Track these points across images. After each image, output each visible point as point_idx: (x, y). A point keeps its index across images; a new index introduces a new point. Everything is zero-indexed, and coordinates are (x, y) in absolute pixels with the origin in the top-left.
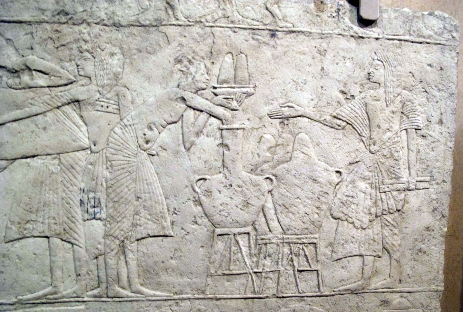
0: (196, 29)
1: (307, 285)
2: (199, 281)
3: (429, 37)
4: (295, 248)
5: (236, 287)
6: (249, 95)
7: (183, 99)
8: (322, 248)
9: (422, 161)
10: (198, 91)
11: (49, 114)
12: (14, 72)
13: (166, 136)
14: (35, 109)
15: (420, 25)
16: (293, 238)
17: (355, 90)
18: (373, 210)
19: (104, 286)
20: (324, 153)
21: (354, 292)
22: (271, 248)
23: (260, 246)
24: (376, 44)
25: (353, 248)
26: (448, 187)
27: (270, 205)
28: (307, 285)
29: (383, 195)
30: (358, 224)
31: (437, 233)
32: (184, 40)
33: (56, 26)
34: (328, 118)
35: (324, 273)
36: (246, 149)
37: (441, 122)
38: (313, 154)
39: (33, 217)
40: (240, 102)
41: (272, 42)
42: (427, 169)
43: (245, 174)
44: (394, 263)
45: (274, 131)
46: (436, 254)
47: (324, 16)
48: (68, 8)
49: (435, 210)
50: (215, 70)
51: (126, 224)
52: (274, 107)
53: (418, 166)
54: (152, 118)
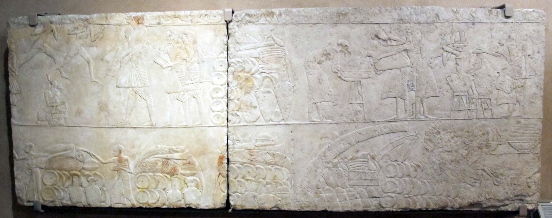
0: (447, 24)
1: (488, 114)
2: (448, 113)
3: (533, 20)
4: (483, 100)
5: (462, 115)
6: (465, 46)
7: (443, 49)
8: (493, 101)
9: (531, 68)
10: (447, 45)
11: (397, 55)
12: (385, 41)
13: (437, 61)
14: (392, 53)
15: (529, 16)
16: (482, 97)
17: (504, 42)
18: (512, 86)
19: (414, 115)
20: (492, 66)
21: (506, 118)
22: (474, 101)
23: (470, 100)
24: (511, 25)
25: (505, 101)
26: (543, 77)
27: (473, 85)
28: (488, 114)
29: (516, 81)
30: (506, 91)
31: (539, 96)
32: (442, 28)
33: (399, 24)
34: (494, 53)
35: (495, 110)
36: (464, 65)
37: (539, 52)
38: (489, 67)
39: (391, 90)
40: (462, 48)
41: (473, 27)
42: (534, 71)
43: (465, 74)
44: (521, 107)
45: (474, 58)
46: (539, 103)
47: (492, 16)
48: (403, 18)
49: (537, 86)
50: (453, 38)
51: (423, 92)
52: (474, 50)
53: (530, 69)
54: (433, 55)
